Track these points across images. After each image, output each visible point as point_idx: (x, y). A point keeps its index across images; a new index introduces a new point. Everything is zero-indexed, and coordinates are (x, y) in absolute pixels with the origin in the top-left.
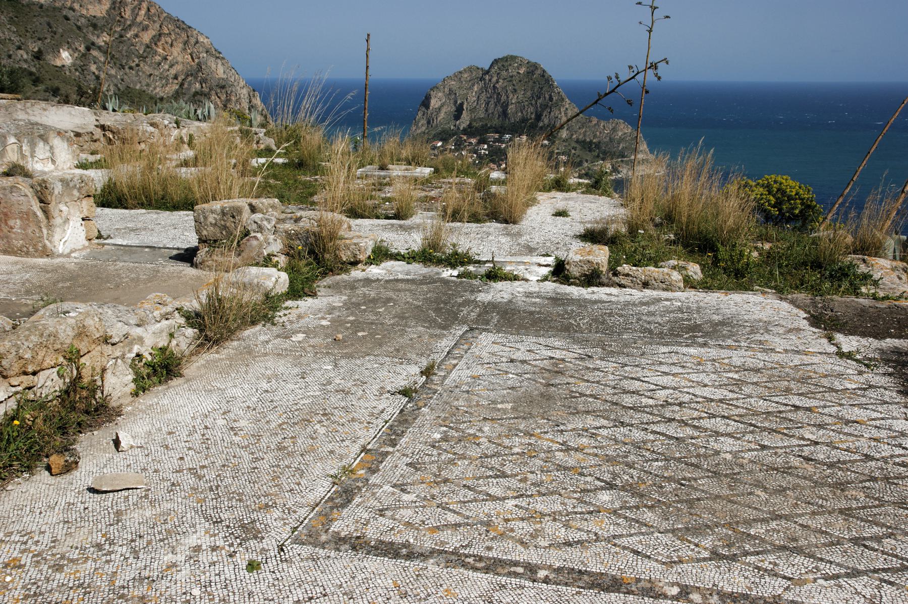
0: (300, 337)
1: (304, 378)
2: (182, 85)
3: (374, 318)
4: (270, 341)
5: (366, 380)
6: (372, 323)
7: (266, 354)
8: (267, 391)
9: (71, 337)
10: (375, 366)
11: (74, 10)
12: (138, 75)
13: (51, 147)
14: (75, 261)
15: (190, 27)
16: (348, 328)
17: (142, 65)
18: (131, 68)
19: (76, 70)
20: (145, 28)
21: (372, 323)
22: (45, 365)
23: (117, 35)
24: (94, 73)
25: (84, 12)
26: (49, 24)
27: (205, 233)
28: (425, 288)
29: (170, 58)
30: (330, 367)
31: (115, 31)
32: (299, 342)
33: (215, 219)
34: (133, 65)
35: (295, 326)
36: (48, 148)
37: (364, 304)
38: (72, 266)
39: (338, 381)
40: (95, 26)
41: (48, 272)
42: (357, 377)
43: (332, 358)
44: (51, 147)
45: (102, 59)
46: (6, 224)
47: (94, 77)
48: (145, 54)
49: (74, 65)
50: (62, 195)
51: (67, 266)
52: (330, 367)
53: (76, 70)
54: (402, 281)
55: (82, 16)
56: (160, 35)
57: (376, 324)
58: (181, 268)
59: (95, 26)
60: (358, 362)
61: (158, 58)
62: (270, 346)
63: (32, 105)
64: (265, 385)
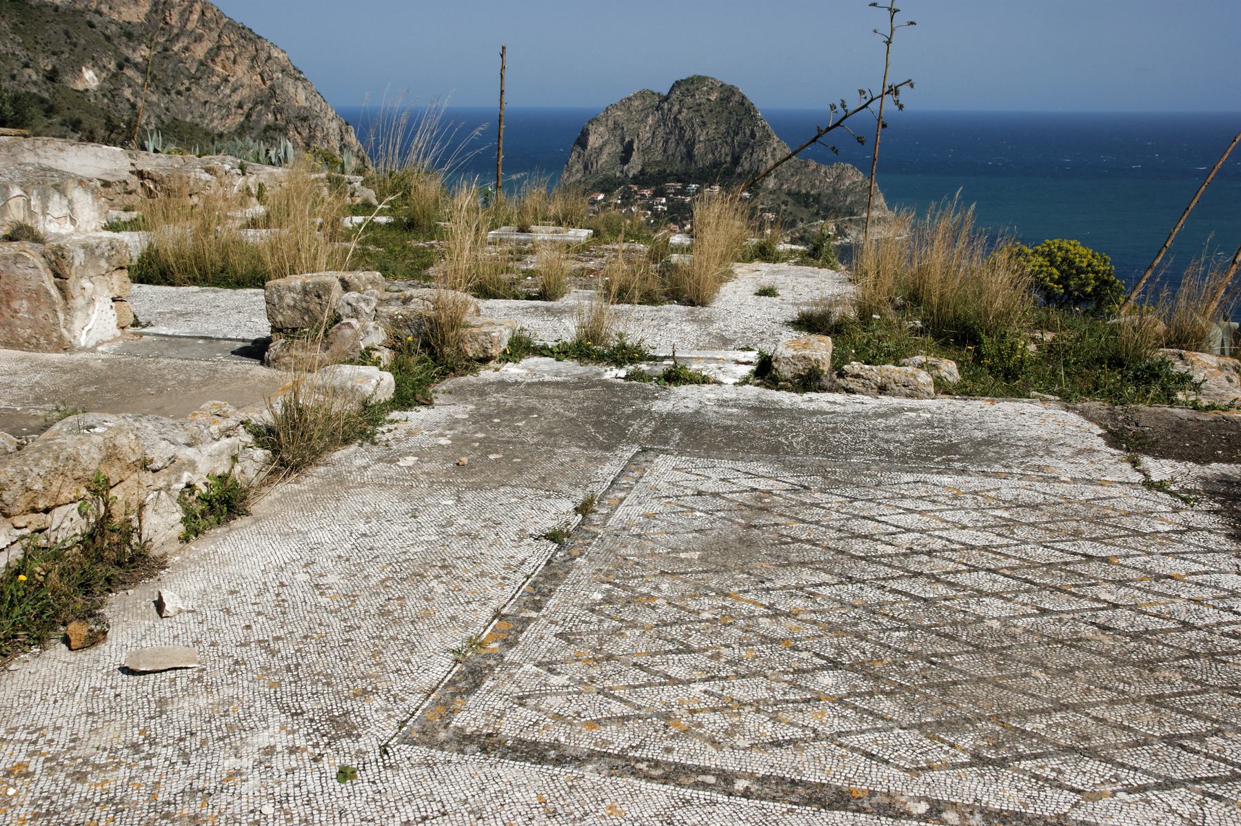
0: (411, 460)
1: (415, 517)
2: (248, 116)
3: (512, 434)
4: (369, 466)
5: (500, 519)
6: (509, 442)
7: (363, 485)
8: (365, 535)
9: (98, 461)
10: (513, 500)
11: (101, 14)
12: (188, 103)
13: (70, 202)
14: (103, 356)
15: (259, 37)
16: (475, 449)
17: (193, 89)
18: (179, 93)
19: (104, 95)
20: (199, 39)
21: (509, 442)
22: (62, 499)
23: (159, 49)
24: (128, 100)
25: (115, 16)
26: (67, 33)
27: (280, 318)
28: (581, 393)
29: (232, 80)
30: (450, 502)
31: (158, 43)
32: (409, 468)
33: (294, 299)
34: (182, 88)
35: (403, 446)
36: (65, 202)
37: (498, 415)
38: (98, 364)
39: (461, 521)
40: (129, 36)
41: (65, 372)
42: (488, 516)
43: (454, 490)
44: (70, 202)
45: (140, 81)
46: (9, 306)
47: (128, 106)
48: (198, 74)
49: (101, 88)
50: (85, 267)
51: (92, 364)
52: (450, 502)
53: (104, 95)
54: (549, 384)
55: (112, 22)
56: (219, 48)
57: (514, 444)
58: (248, 367)
59: (129, 36)
60: (489, 495)
61: (216, 80)
62: (369, 473)
63: (44, 144)
64: (362, 527)
